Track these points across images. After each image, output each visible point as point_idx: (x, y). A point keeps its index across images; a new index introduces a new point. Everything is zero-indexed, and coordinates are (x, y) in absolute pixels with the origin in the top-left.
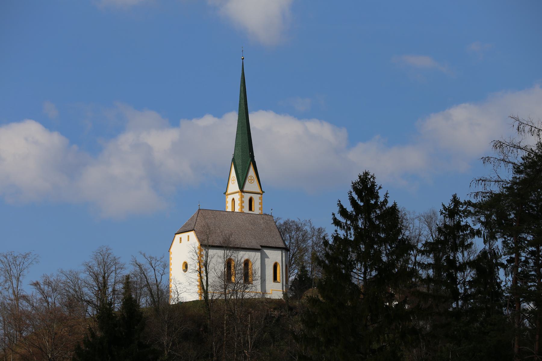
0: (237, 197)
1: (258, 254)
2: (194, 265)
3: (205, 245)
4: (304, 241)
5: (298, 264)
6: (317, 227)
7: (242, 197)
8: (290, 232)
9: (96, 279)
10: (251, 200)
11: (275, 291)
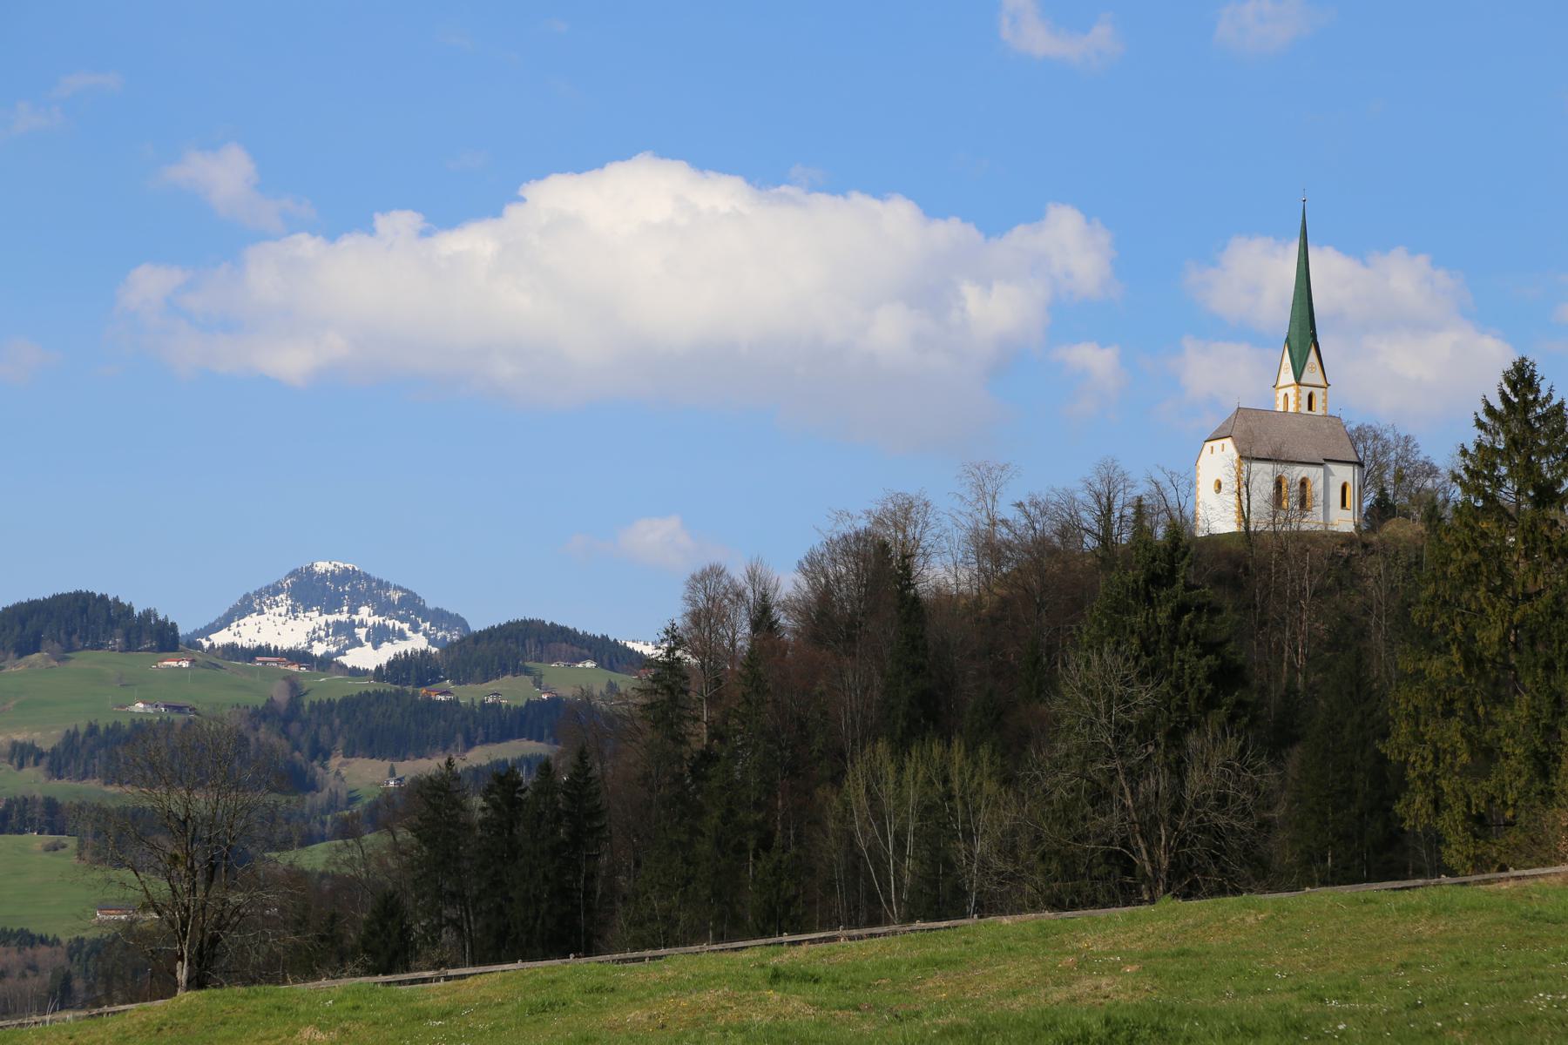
0: (1291, 391)
1: (1321, 470)
2: (1230, 484)
3: (1246, 457)
4: (1384, 453)
5: (1376, 485)
6: (1403, 435)
7: (1298, 392)
8: (1365, 441)
9: (1098, 497)
10: (1310, 397)
11: (1344, 521)
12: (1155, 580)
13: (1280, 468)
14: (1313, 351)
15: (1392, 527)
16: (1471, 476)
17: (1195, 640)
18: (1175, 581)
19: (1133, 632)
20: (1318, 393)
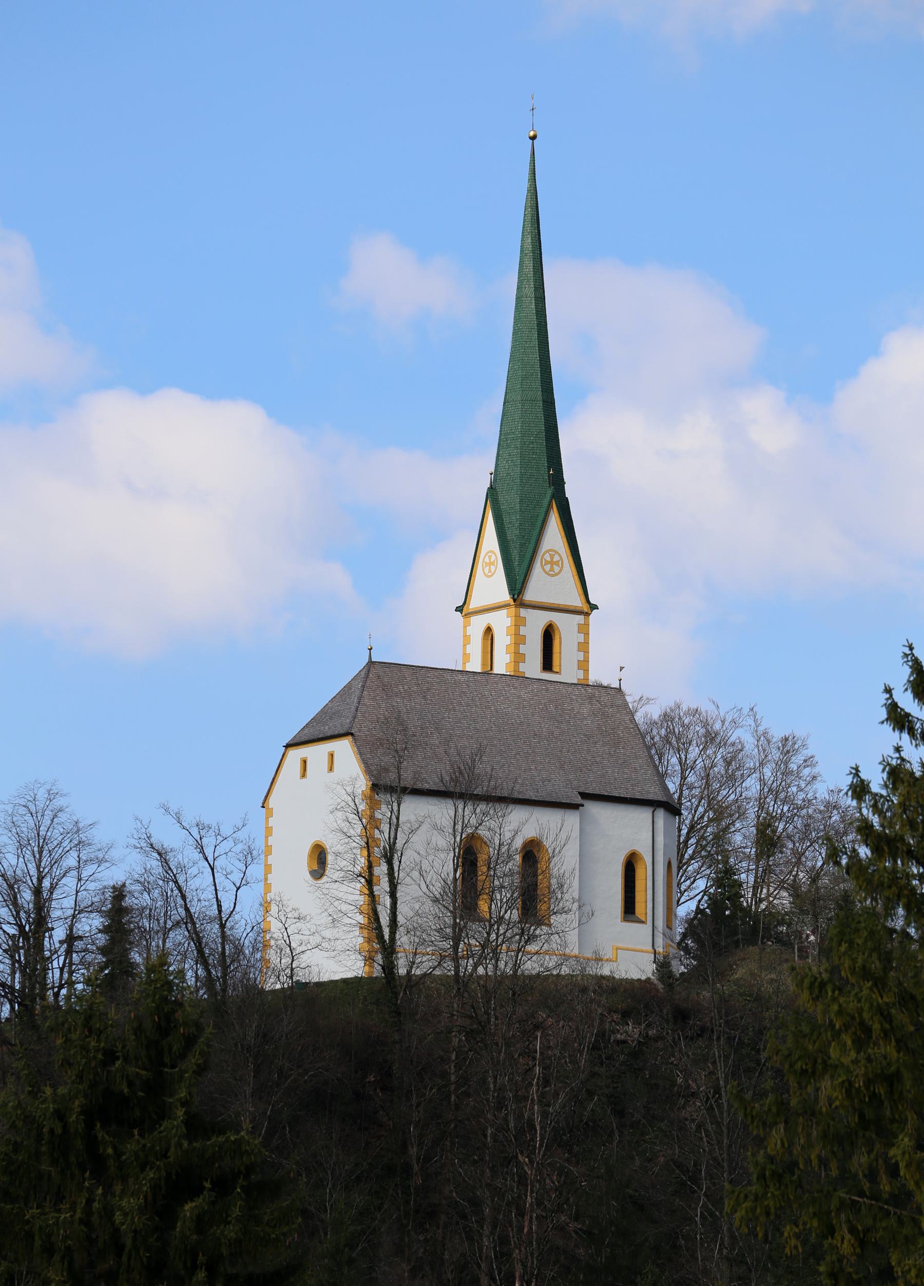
0: (501, 622)
1: (572, 819)
2: (347, 856)
3: (387, 786)
4: (731, 779)
6: (777, 734)
7: (519, 622)
8: (682, 746)
10: (549, 636)
11: (630, 952)
12: (110, 1109)
13: (470, 813)
14: (554, 524)
15: (748, 969)
16: (877, 850)
17: (211, 1269)
18: (163, 1113)
19: (49, 1250)
20: (566, 625)
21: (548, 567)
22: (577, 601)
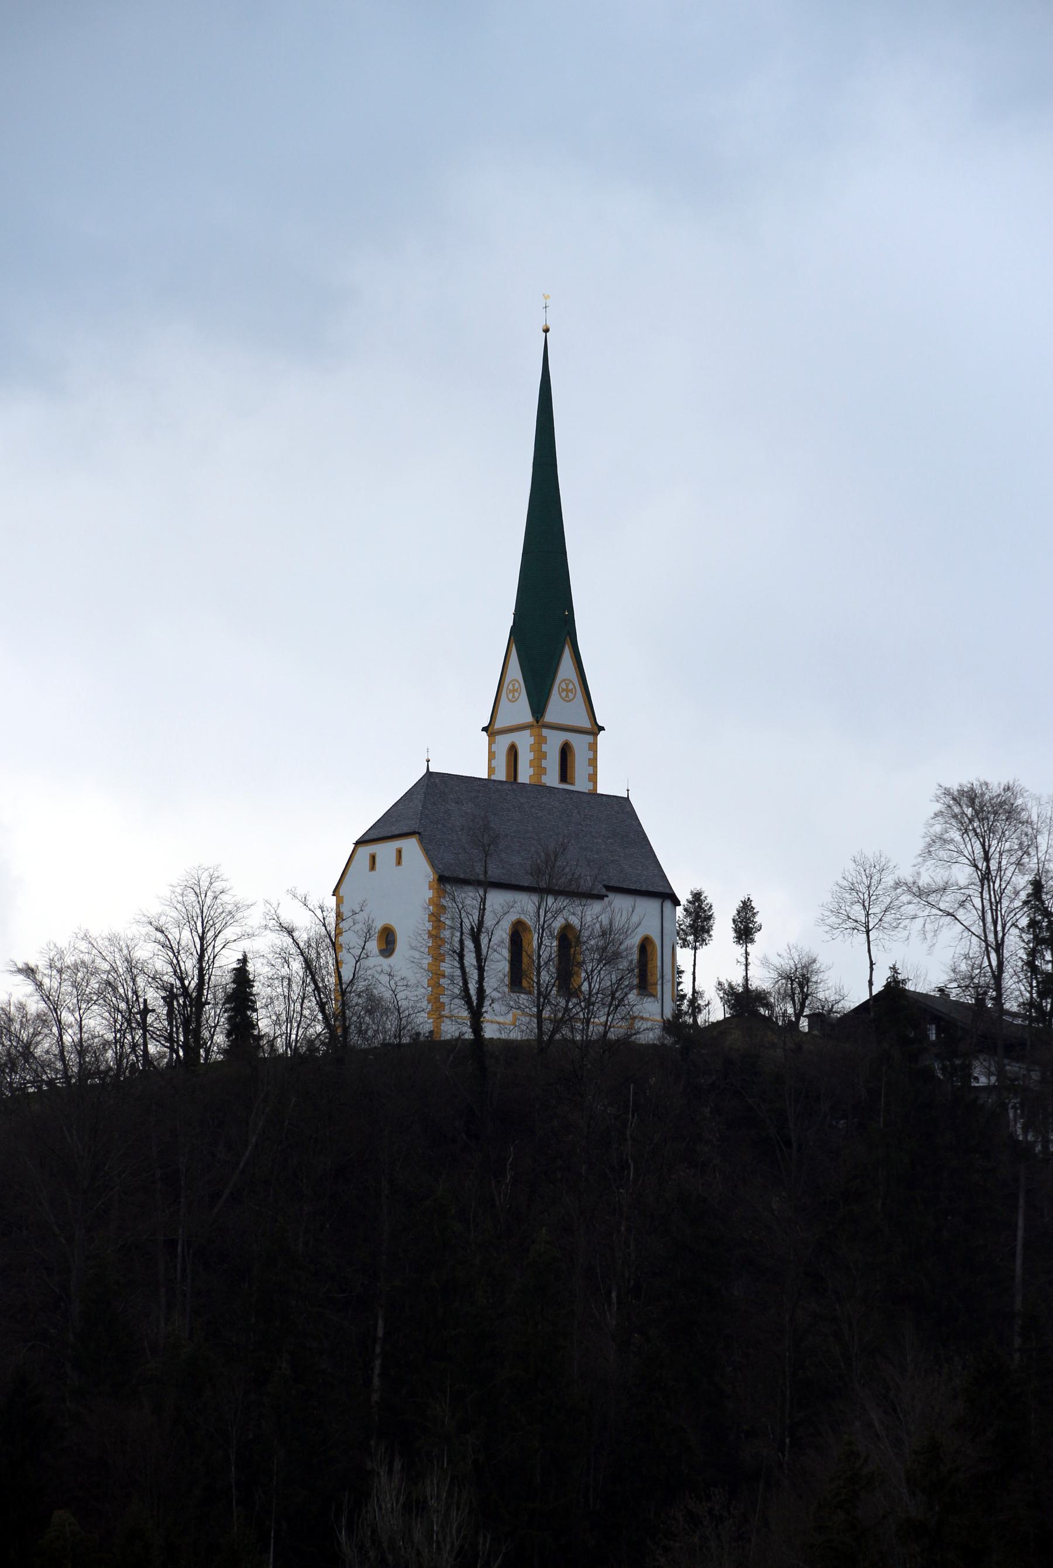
20: (579, 743)
21: (564, 694)
22: (587, 724)
